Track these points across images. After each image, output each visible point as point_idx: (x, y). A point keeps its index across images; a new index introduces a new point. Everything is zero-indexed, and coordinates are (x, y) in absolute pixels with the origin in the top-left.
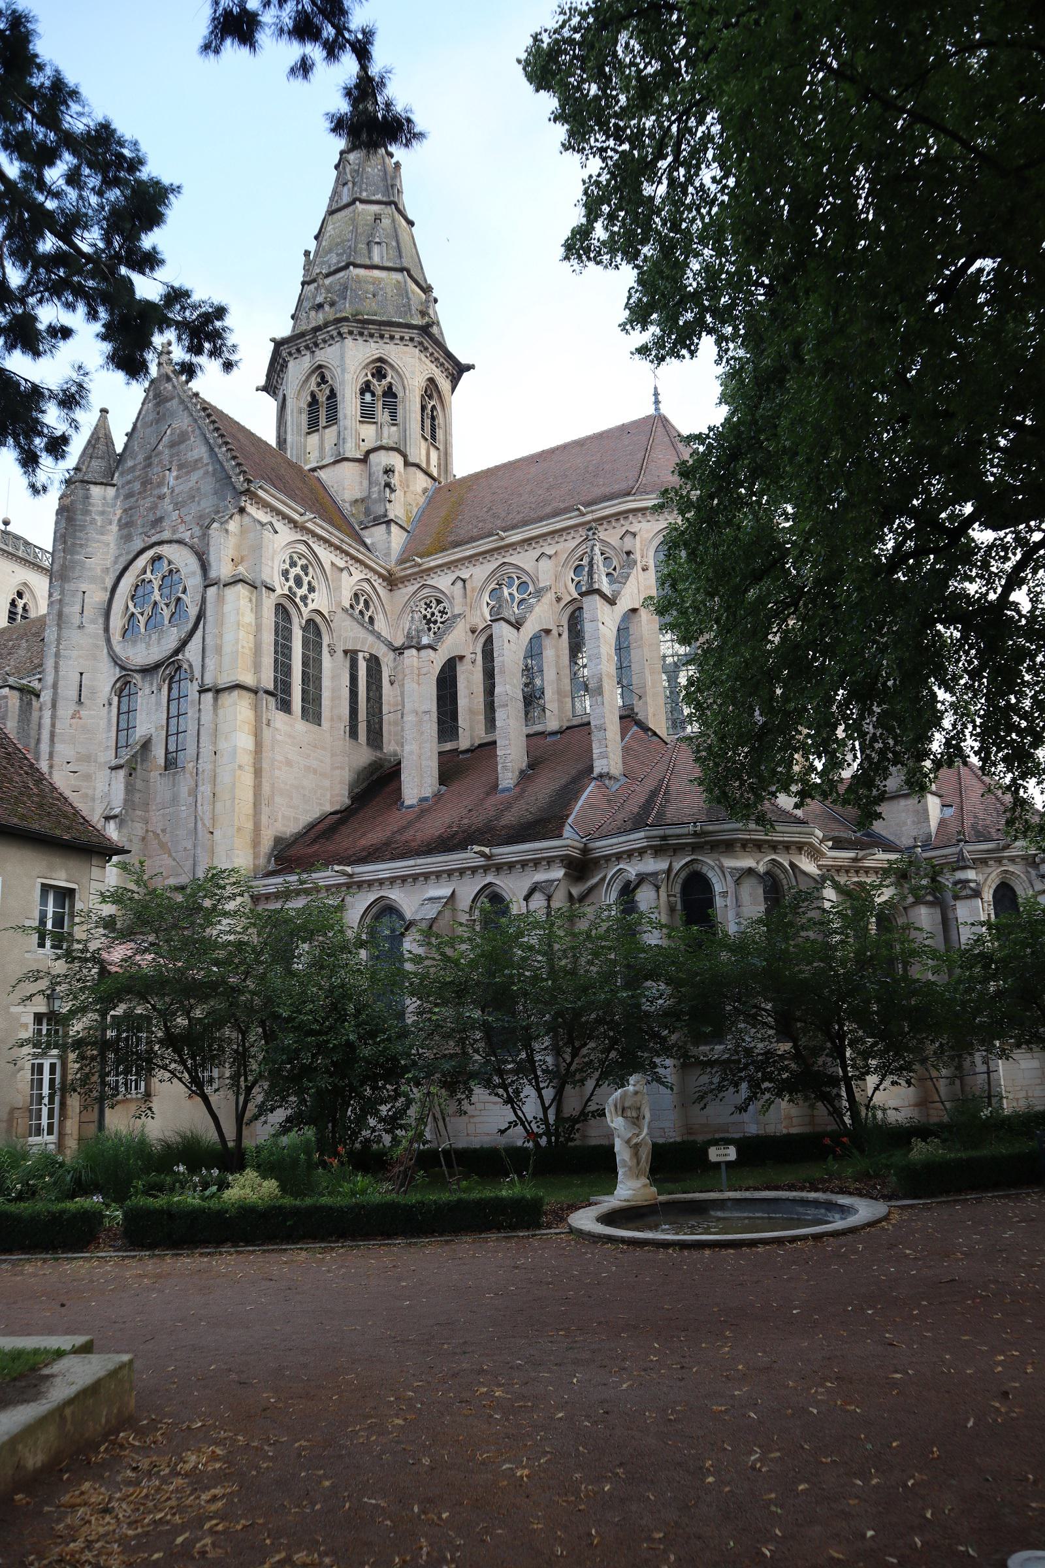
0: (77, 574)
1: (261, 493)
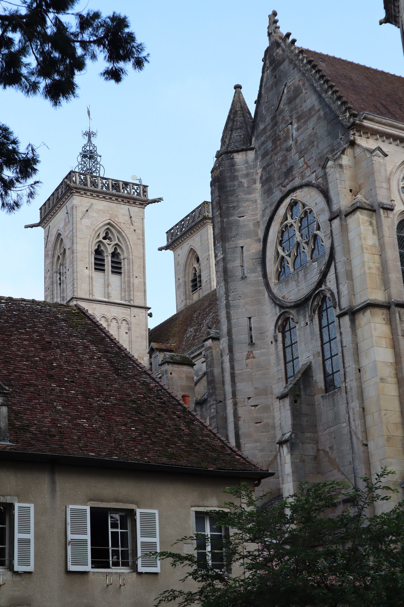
0: (234, 233)
1: (366, 123)
